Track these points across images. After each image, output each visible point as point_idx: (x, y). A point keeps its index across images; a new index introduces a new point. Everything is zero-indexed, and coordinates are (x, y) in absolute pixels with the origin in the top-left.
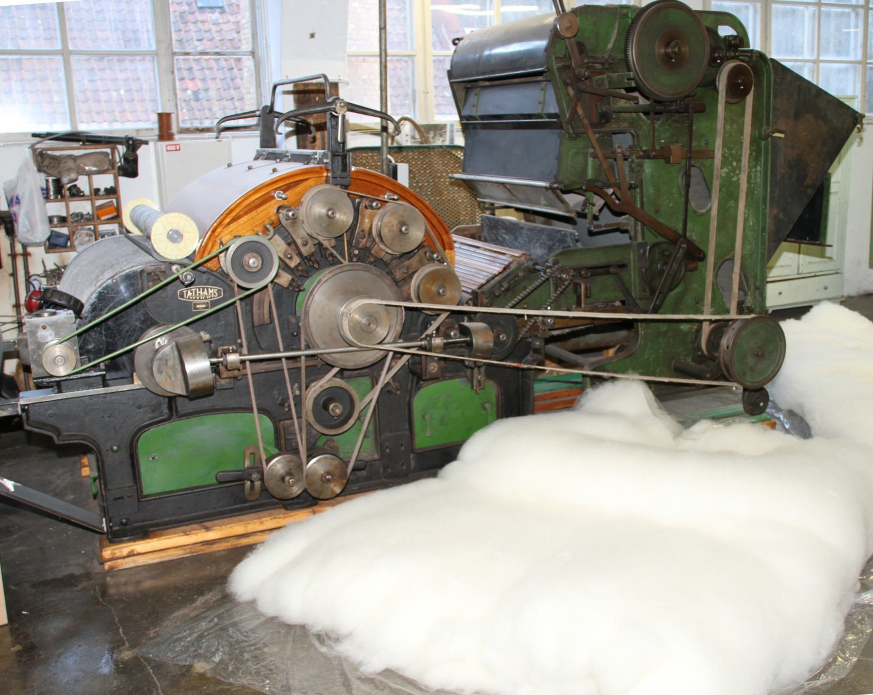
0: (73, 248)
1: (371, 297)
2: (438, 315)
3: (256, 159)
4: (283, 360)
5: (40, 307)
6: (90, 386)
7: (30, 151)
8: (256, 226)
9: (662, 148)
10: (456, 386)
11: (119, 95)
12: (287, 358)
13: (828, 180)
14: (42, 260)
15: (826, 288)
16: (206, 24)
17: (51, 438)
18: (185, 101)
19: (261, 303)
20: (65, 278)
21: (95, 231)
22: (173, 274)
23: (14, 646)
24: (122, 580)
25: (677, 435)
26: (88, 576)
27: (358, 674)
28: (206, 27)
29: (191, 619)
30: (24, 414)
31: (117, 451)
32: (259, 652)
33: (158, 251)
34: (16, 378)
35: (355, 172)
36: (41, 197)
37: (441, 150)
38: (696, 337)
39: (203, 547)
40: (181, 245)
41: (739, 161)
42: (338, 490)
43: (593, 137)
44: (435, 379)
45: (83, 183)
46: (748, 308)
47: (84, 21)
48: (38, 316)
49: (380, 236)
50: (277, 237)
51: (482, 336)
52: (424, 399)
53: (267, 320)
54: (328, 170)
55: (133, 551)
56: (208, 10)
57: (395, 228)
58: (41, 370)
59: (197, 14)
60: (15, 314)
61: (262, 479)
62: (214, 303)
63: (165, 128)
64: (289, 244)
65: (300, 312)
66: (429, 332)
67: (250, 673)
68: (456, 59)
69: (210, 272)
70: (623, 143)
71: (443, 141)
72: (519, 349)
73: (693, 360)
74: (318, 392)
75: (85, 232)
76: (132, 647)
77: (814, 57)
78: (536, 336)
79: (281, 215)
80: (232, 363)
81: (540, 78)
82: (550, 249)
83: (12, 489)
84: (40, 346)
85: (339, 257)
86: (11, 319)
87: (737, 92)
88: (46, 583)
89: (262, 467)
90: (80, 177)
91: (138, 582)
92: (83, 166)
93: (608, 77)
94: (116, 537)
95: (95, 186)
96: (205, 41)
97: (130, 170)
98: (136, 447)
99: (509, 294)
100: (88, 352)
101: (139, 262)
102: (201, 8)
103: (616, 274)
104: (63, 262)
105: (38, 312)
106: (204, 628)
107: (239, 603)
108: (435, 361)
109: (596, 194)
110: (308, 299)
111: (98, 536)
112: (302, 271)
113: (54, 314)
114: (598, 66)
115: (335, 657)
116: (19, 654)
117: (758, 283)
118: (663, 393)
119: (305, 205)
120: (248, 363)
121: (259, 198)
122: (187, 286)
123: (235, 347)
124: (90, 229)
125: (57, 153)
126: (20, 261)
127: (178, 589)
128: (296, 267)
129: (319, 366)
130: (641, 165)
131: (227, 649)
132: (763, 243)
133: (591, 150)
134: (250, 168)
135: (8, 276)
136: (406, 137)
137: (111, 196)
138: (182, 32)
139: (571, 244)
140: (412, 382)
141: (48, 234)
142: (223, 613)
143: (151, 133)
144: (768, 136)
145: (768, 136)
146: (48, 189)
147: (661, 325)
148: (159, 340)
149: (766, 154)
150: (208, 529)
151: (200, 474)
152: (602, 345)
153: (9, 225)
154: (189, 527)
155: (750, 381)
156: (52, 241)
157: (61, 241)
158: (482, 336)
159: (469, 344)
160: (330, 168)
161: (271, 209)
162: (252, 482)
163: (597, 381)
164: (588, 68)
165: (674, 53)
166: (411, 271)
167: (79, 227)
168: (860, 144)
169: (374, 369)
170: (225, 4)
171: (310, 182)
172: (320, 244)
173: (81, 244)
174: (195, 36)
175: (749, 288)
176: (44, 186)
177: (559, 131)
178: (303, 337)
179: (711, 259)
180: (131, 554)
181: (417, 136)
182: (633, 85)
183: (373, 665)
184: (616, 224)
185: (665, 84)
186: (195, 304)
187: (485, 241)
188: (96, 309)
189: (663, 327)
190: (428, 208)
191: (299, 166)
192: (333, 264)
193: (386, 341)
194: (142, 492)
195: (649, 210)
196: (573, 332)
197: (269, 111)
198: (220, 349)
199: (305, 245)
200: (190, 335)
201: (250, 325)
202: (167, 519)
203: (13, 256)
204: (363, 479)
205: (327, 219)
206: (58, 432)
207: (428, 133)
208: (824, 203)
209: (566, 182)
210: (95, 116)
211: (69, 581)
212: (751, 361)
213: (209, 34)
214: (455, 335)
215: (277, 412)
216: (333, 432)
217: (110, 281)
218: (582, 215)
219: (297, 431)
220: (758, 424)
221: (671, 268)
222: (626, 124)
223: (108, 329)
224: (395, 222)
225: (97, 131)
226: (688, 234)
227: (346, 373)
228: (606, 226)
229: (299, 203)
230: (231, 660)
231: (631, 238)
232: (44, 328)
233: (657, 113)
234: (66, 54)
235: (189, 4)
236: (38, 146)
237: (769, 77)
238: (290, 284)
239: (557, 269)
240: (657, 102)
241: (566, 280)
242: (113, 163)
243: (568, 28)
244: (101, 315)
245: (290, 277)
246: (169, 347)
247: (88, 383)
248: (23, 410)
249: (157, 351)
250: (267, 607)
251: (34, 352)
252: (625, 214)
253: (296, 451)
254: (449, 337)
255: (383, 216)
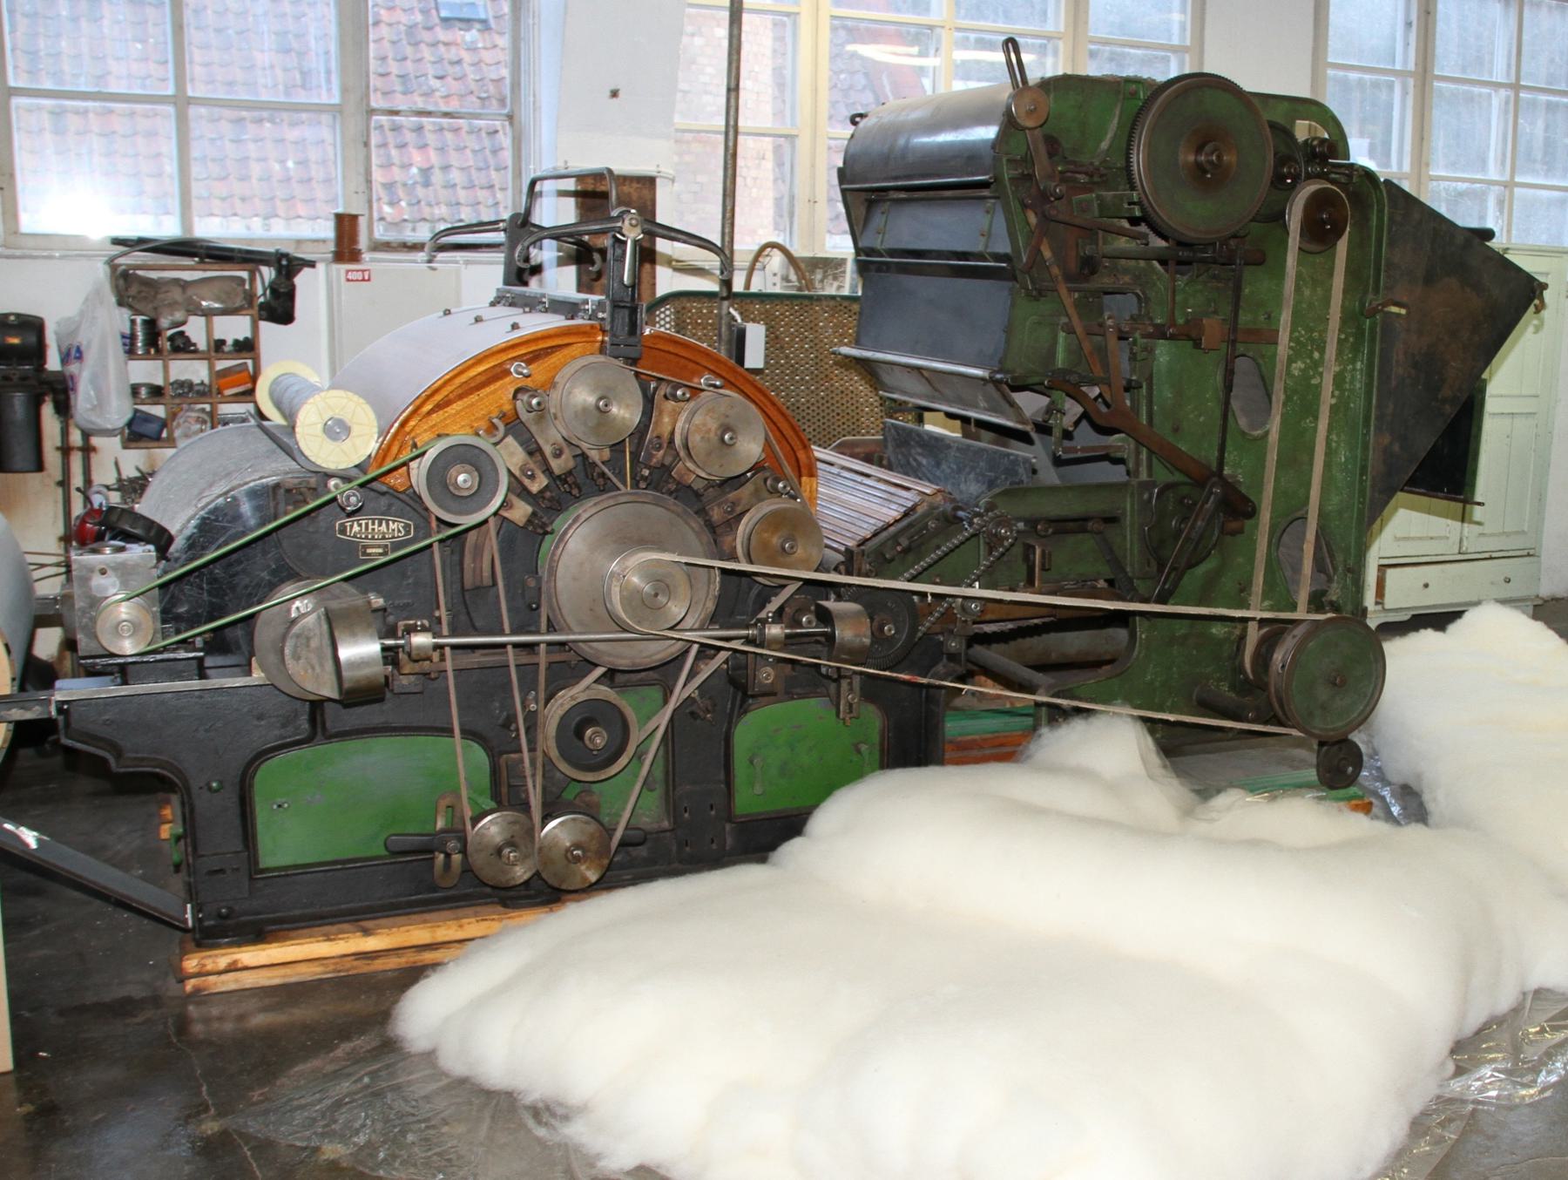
0: (171, 443)
1: (664, 550)
2: (784, 586)
3: (493, 304)
4: (509, 648)
5: (100, 537)
6: (179, 676)
7: (108, 269)
8: (477, 419)
9: (1187, 322)
10: (810, 711)
11: (287, 170)
12: (516, 645)
13: (1483, 391)
14: (115, 460)
15: (1508, 581)
16: (453, 50)
17: (104, 761)
18: (405, 185)
19: (478, 550)
20: (149, 491)
21: (212, 414)
22: (329, 491)
23: (21, 1105)
24: (215, 1012)
25: (1187, 813)
26: (156, 1000)
27: (594, 1172)
28: (453, 54)
29: (325, 1076)
30: (61, 718)
31: (216, 791)
32: (432, 1132)
33: (307, 453)
34: (57, 667)
35: (651, 336)
36: (120, 350)
37: (832, 303)
38: (1238, 649)
39: (356, 963)
40: (347, 445)
41: (1322, 351)
42: (593, 876)
43: (1068, 299)
44: (769, 694)
45: (195, 330)
46: (1332, 603)
47: (230, 31)
48: (95, 551)
49: (686, 447)
50: (510, 440)
51: (851, 628)
52: (753, 729)
53: (487, 581)
54: (604, 332)
55: (235, 962)
56: (458, 24)
57: (712, 435)
58: (93, 645)
59: (438, 29)
60: (61, 551)
61: (464, 851)
62: (397, 546)
63: (346, 242)
64: (531, 454)
65: (544, 573)
66: (762, 615)
67: (415, 1165)
68: (851, 151)
69: (392, 493)
70: (1118, 310)
71: (839, 287)
72: (922, 652)
73: (1232, 687)
74: (567, 707)
75: (194, 415)
76: (221, 1115)
77: (1506, 177)
78: (951, 632)
79: (519, 403)
80: (419, 648)
81: (986, 193)
82: (991, 484)
83: (33, 845)
84: (95, 602)
85: (615, 480)
86: (53, 560)
87: (1320, 231)
88: (83, 1009)
89: (464, 831)
90: (192, 319)
91: (241, 1018)
92: (203, 298)
93: (1098, 197)
94: (208, 936)
95: (217, 336)
96: (449, 79)
97: (280, 310)
98: (251, 786)
99: (910, 558)
100: (178, 618)
101: (275, 470)
102: (445, 20)
103: (1099, 533)
104: (152, 466)
105: (94, 546)
106: (345, 1091)
107: (410, 1055)
108: (770, 664)
109: (1068, 395)
110: (557, 547)
111: (179, 934)
112: (551, 499)
113: (122, 549)
114: (1083, 178)
115: (559, 1145)
116: (29, 1118)
117: (1351, 562)
118: (1174, 745)
119: (560, 387)
120: (447, 650)
121: (486, 371)
122: (350, 514)
123: (426, 623)
124: (203, 410)
125: (154, 275)
126: (76, 461)
127: (307, 1028)
128: (541, 491)
129: (570, 664)
130: (1150, 351)
131: (379, 1126)
132: (1362, 492)
133: (1064, 320)
134: (478, 320)
135: (53, 485)
136: (771, 279)
137: (244, 354)
138: (409, 63)
139: (1024, 478)
140: (734, 698)
141: (129, 415)
142: (379, 1070)
143: (322, 248)
144: (1373, 313)
145: (1373, 313)
146: (133, 337)
147: (1177, 623)
148: (300, 604)
149: (1373, 340)
150: (367, 932)
151: (356, 838)
152: (1091, 658)
153: (62, 397)
154: (334, 928)
155: (1320, 725)
156: (134, 428)
157: (151, 428)
158: (851, 628)
159: (830, 638)
160: (608, 328)
161: (500, 394)
162: (448, 856)
163: (1058, 715)
164: (1063, 180)
165: (1211, 163)
166: (739, 510)
167: (185, 406)
168: (1537, 329)
169: (664, 672)
170: (491, 14)
171: (575, 350)
172: (584, 456)
173: (187, 436)
174: (431, 71)
175: (1335, 569)
176: (128, 331)
177: (1010, 284)
178: (544, 612)
179: (1265, 516)
180: (233, 968)
181: (793, 277)
182: (1138, 213)
183: (622, 1157)
184: (1106, 447)
185: (1194, 214)
186: (365, 547)
187: (890, 468)
188: (195, 545)
189: (1181, 628)
190: (774, 404)
191: (556, 321)
192: (603, 491)
193: (688, 623)
194: (256, 863)
195: (1163, 429)
196: (1020, 628)
197: (522, 226)
198: (401, 624)
199: (558, 454)
200: (351, 597)
201: (457, 586)
202: (297, 912)
203: (66, 450)
204: (635, 861)
205: (596, 412)
206: (119, 753)
207: (812, 272)
208: (1474, 430)
209: (1019, 372)
210: (238, 203)
211: (124, 1008)
212: (1323, 693)
213: (457, 68)
214: (809, 622)
215: (496, 739)
216: (589, 777)
217: (221, 500)
218: (1044, 429)
219: (528, 772)
220: (1327, 803)
221: (1193, 527)
222: (1127, 279)
223: (213, 580)
224: (713, 425)
225: (227, 240)
226: (1227, 471)
227: (620, 678)
228: (1083, 450)
229: (551, 384)
230: (384, 1142)
231: (1128, 473)
232: (103, 572)
233: (1180, 263)
234: (182, 102)
235: (425, 12)
236: (121, 261)
237: (1381, 211)
238: (529, 521)
239: (992, 519)
240: (1180, 244)
241: (1007, 538)
242: (250, 297)
243: (1030, 113)
244: (201, 556)
245: (529, 509)
246: (314, 616)
247: (172, 670)
248: (60, 711)
249: (294, 622)
250: (453, 1063)
251: (84, 611)
252: (1119, 432)
253: (525, 807)
254: (800, 625)
255: (693, 413)
